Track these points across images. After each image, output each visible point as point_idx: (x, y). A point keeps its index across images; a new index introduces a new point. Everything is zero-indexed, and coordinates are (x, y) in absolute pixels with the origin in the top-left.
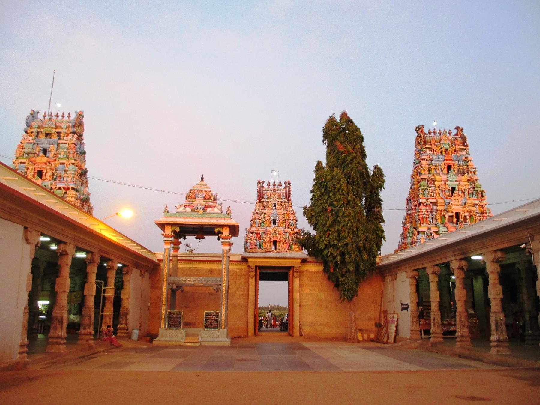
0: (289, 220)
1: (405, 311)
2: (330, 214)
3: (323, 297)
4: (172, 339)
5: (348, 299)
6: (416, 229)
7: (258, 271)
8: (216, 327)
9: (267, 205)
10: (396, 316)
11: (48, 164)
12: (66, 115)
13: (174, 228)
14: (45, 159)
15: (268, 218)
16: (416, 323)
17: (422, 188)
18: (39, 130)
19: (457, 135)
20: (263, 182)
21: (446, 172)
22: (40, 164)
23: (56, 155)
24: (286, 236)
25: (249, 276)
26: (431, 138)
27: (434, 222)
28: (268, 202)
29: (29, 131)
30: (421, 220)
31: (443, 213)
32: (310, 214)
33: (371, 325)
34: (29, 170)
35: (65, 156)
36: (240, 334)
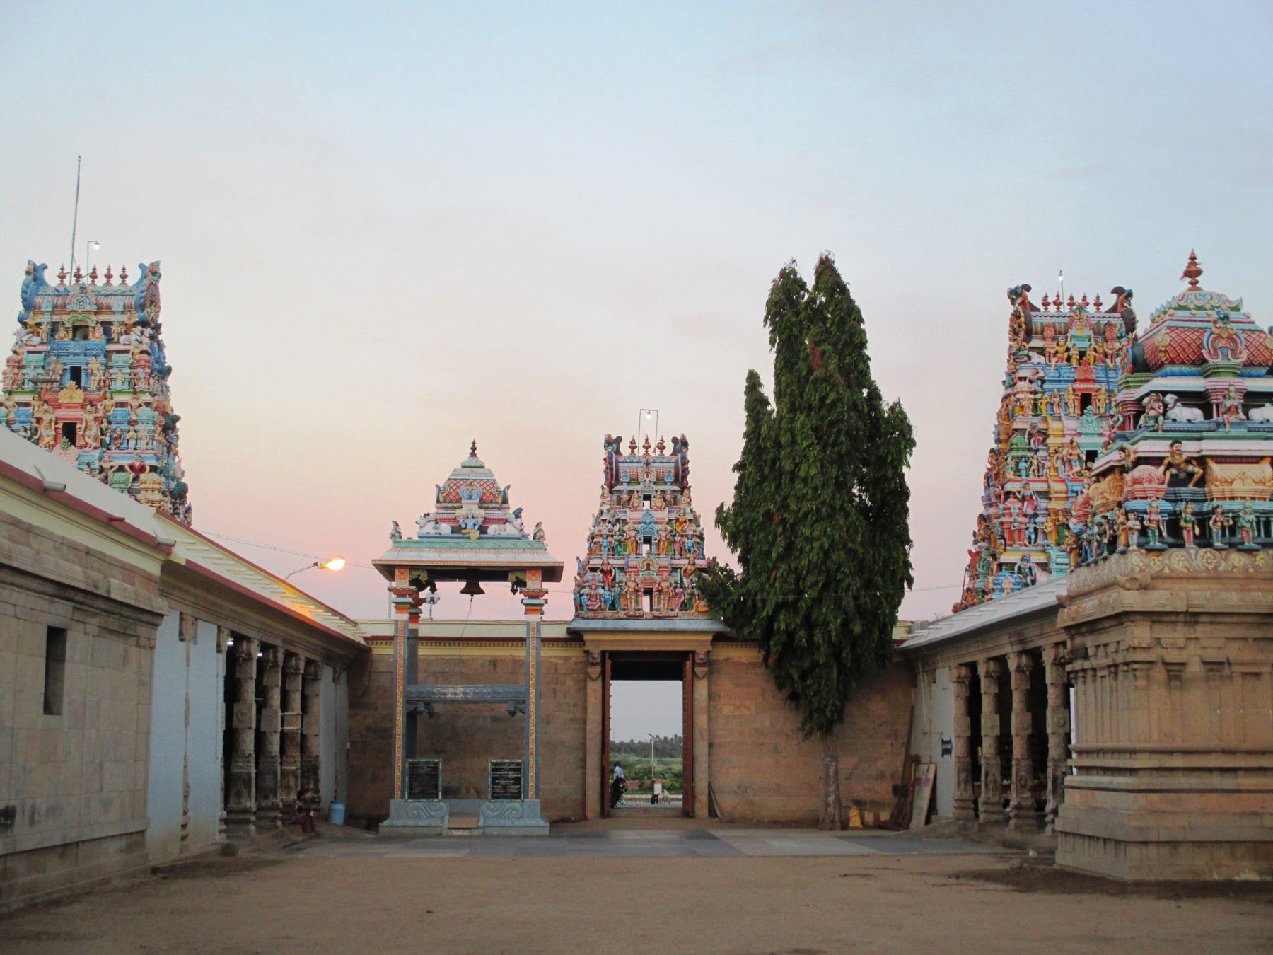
0: (682, 537)
1: (947, 756)
2: (780, 530)
3: (768, 723)
4: (421, 823)
5: (820, 728)
6: (994, 556)
7: (609, 663)
8: (516, 796)
9: (629, 500)
10: (932, 767)
11: (89, 407)
12: (116, 272)
13: (415, 574)
14: (79, 396)
15: (633, 533)
16: (966, 782)
17: (1014, 453)
18: (56, 318)
19: (1114, 309)
20: (619, 440)
21: (1078, 411)
22: (69, 407)
23: (105, 384)
24: (677, 576)
25: (587, 674)
26: (1045, 321)
27: (1040, 541)
28: (631, 492)
29: (31, 322)
30: (1006, 535)
31: (1061, 518)
32: (736, 525)
33: (884, 790)
34: (44, 424)
35: (126, 385)
36: (568, 813)
